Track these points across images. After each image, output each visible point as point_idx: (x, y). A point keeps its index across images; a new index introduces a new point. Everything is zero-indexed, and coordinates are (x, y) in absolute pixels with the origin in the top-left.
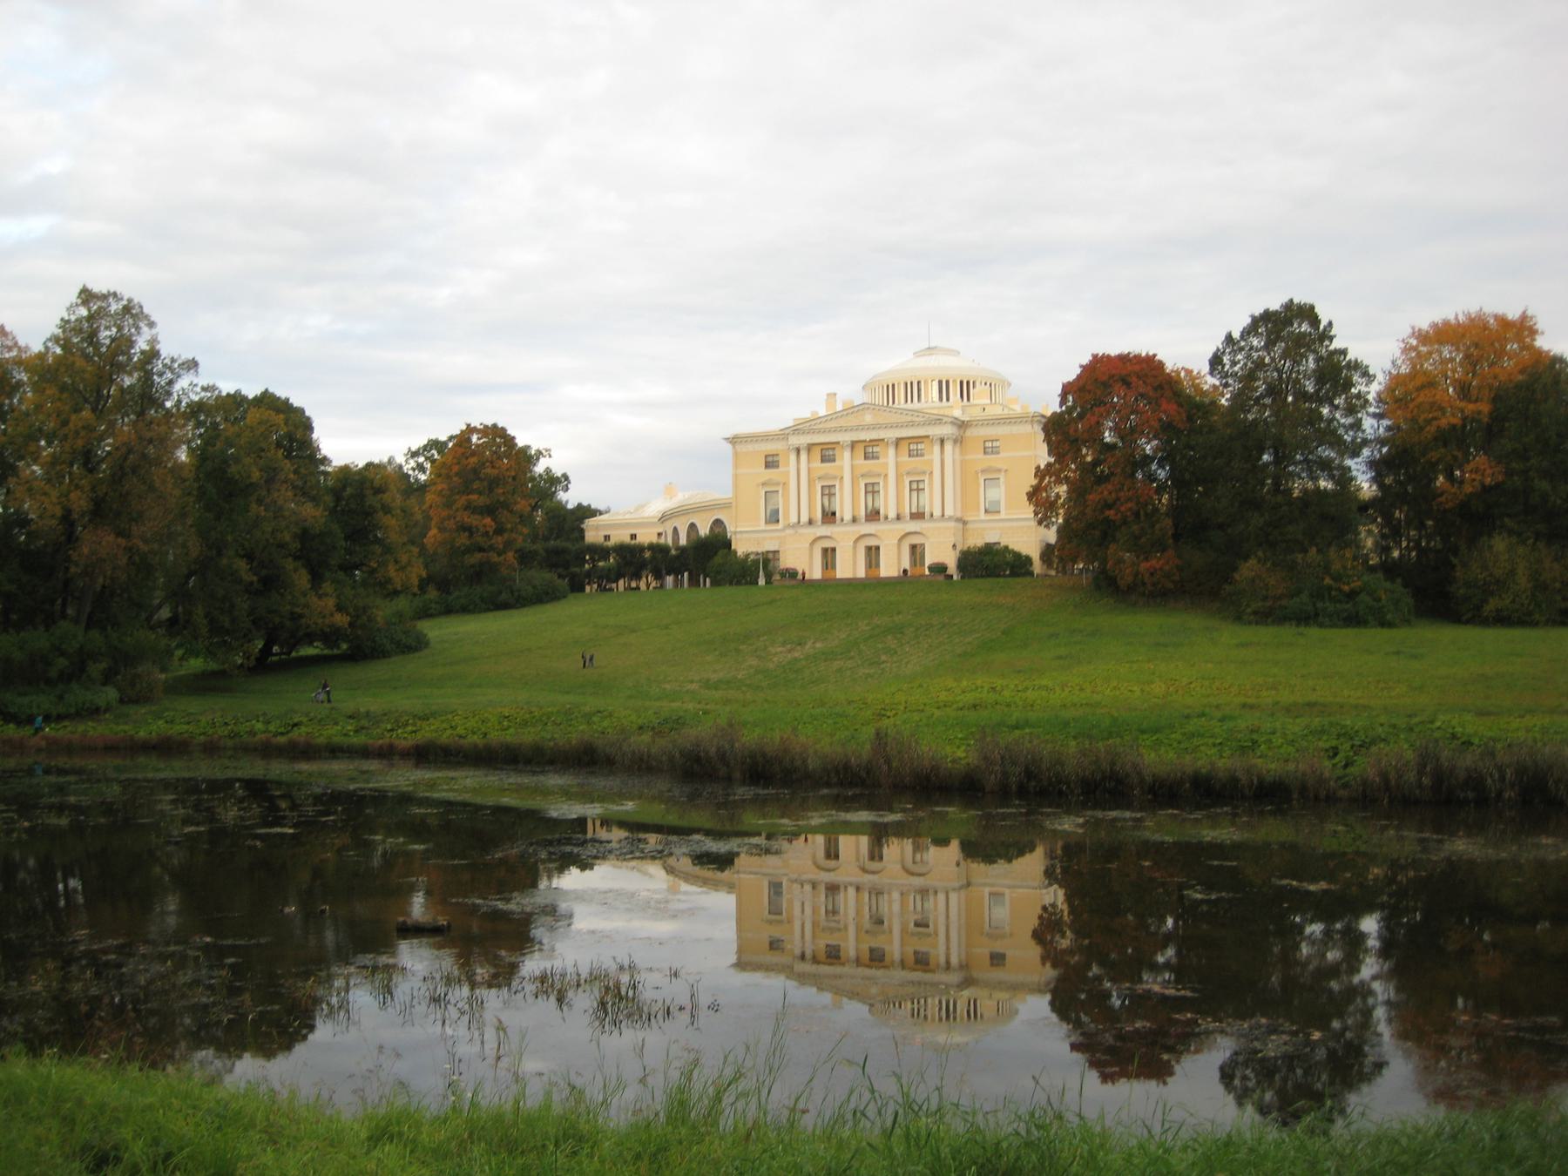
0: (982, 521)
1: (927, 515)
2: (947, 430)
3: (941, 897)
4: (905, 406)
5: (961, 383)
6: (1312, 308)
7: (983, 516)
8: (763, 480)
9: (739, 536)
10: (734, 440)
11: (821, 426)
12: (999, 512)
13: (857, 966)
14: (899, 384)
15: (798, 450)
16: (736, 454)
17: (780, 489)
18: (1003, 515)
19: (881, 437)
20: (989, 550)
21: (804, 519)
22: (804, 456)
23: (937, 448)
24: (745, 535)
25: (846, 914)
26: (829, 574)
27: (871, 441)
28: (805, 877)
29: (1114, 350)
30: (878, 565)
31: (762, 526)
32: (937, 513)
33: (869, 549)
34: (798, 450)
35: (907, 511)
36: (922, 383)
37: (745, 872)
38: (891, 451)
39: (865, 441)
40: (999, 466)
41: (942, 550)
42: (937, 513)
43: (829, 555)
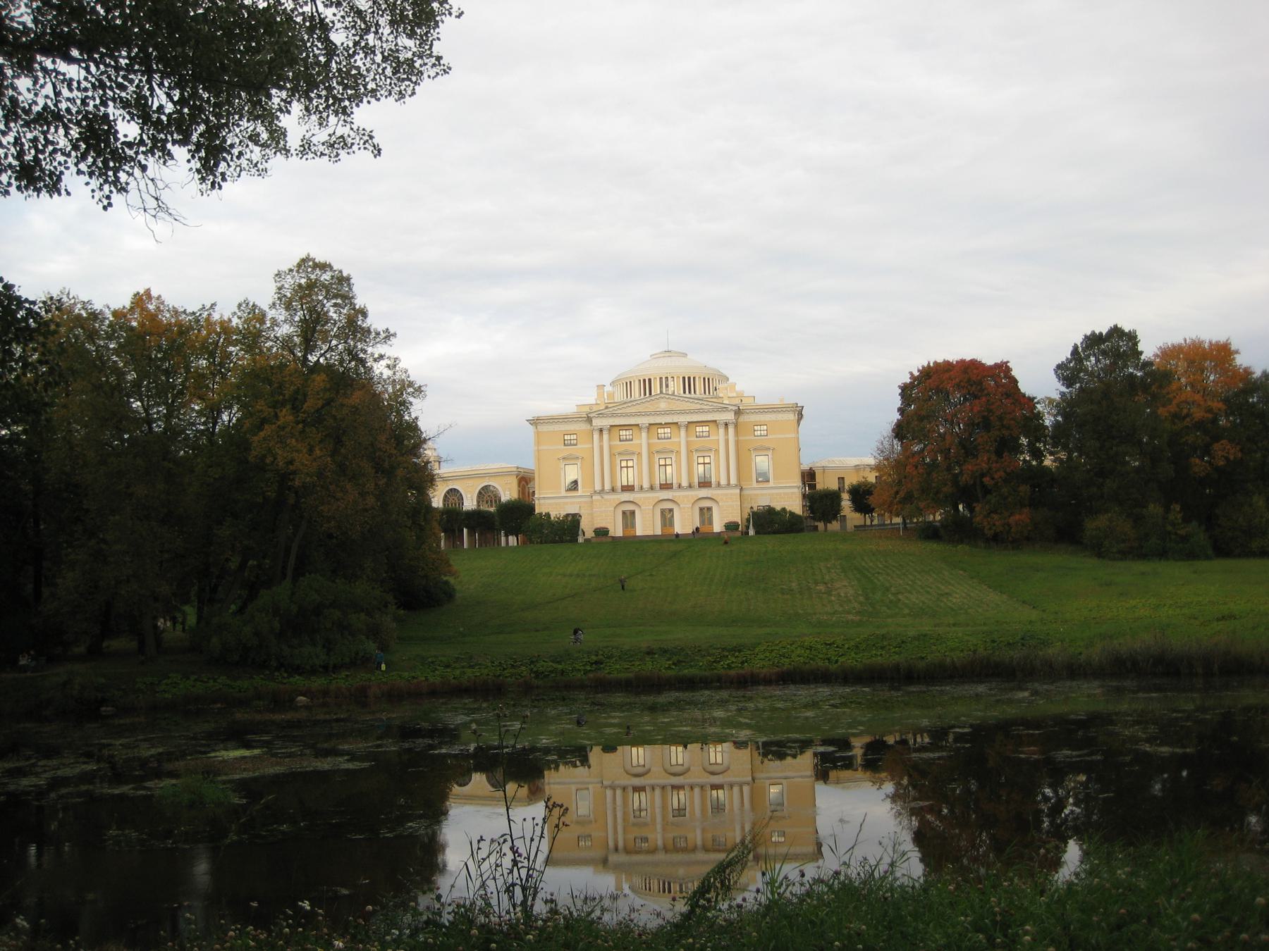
0: (755, 489)
1: (675, 486)
2: (730, 416)
3: (736, 789)
4: (689, 396)
5: (684, 378)
6: (1116, 326)
7: (755, 485)
8: (561, 455)
9: (542, 501)
10: (535, 422)
11: (619, 412)
12: (768, 481)
13: (666, 852)
14: (655, 378)
15: (601, 430)
16: (538, 434)
17: (635, 458)
18: (771, 484)
19: (714, 419)
20: (770, 511)
21: (607, 487)
22: (605, 436)
23: (722, 431)
24: (547, 501)
25: (732, 809)
26: (669, 531)
27: (666, 424)
28: (617, 782)
29: (953, 357)
30: (633, 526)
31: (564, 493)
32: (723, 482)
33: (701, 509)
34: (601, 430)
35: (658, 483)
36: (697, 379)
37: (554, 784)
38: (644, 434)
39: (661, 424)
40: (767, 445)
41: (727, 512)
42: (723, 482)
43: (629, 517)
